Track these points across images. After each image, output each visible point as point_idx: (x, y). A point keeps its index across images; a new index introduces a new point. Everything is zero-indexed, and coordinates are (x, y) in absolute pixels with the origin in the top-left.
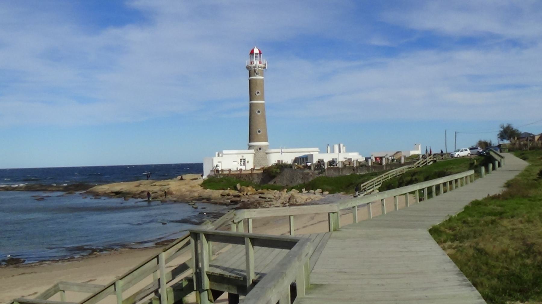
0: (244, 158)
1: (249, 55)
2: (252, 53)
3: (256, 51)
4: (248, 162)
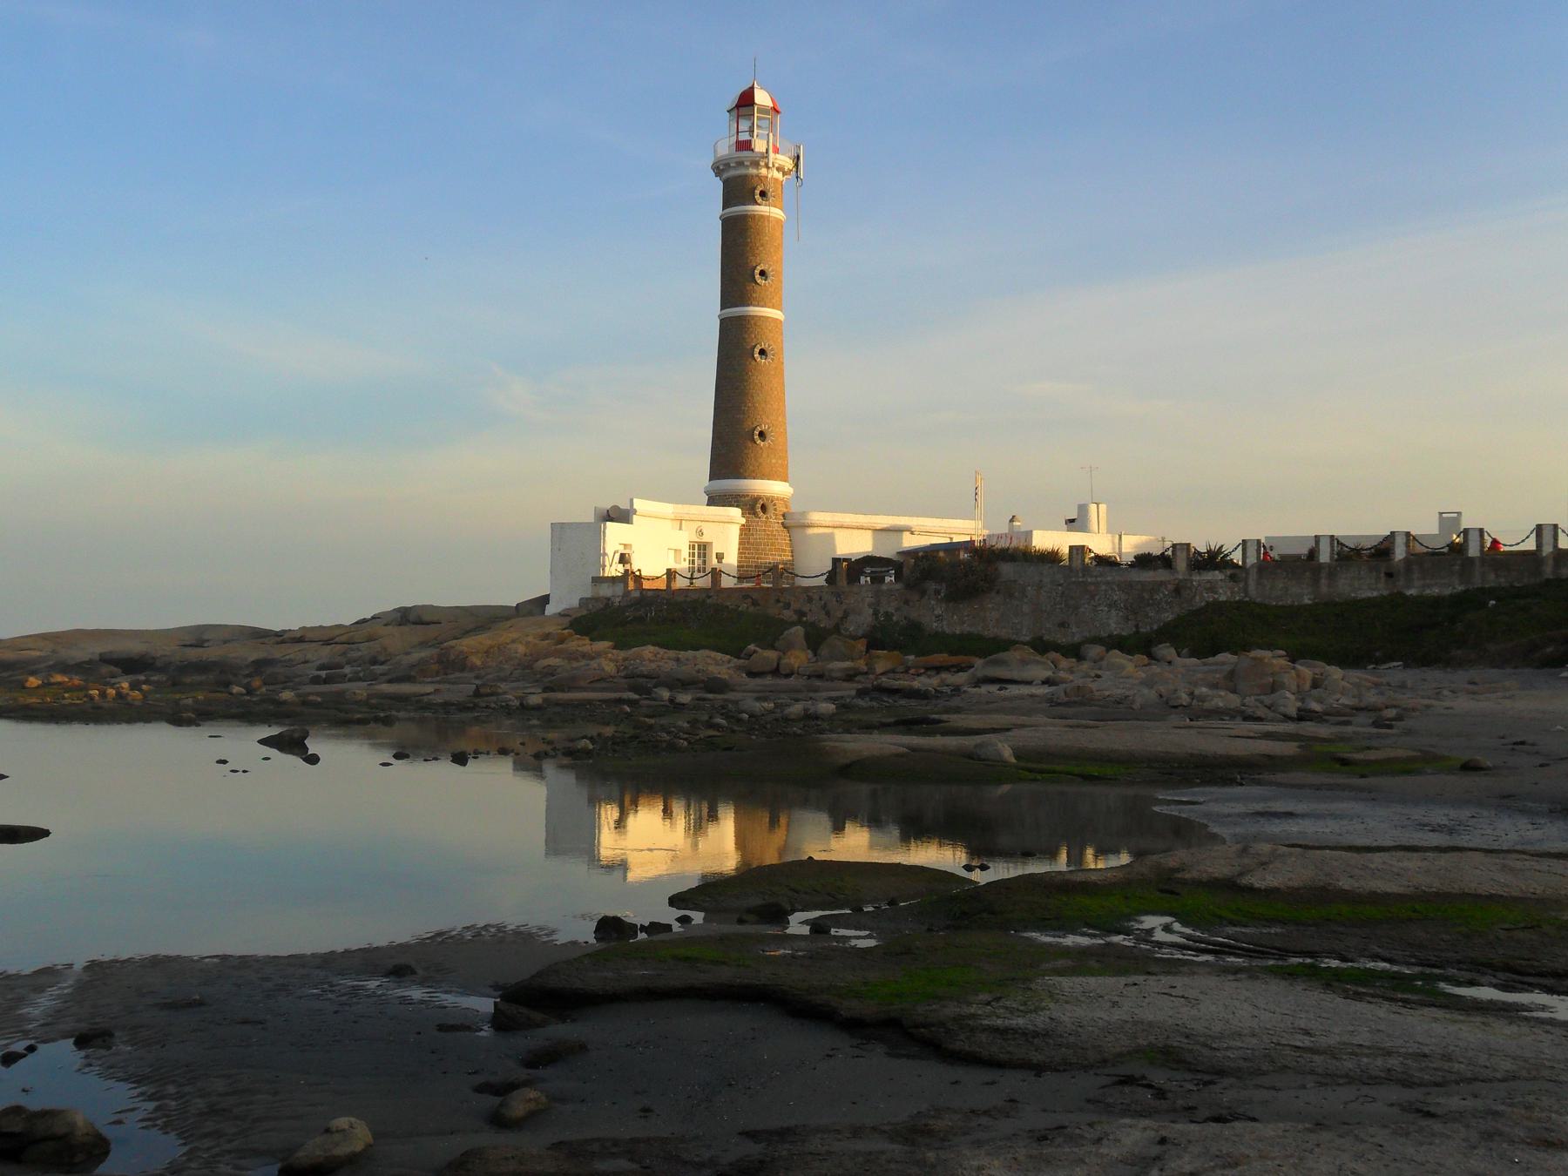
0: (705, 539)
3: (762, 98)
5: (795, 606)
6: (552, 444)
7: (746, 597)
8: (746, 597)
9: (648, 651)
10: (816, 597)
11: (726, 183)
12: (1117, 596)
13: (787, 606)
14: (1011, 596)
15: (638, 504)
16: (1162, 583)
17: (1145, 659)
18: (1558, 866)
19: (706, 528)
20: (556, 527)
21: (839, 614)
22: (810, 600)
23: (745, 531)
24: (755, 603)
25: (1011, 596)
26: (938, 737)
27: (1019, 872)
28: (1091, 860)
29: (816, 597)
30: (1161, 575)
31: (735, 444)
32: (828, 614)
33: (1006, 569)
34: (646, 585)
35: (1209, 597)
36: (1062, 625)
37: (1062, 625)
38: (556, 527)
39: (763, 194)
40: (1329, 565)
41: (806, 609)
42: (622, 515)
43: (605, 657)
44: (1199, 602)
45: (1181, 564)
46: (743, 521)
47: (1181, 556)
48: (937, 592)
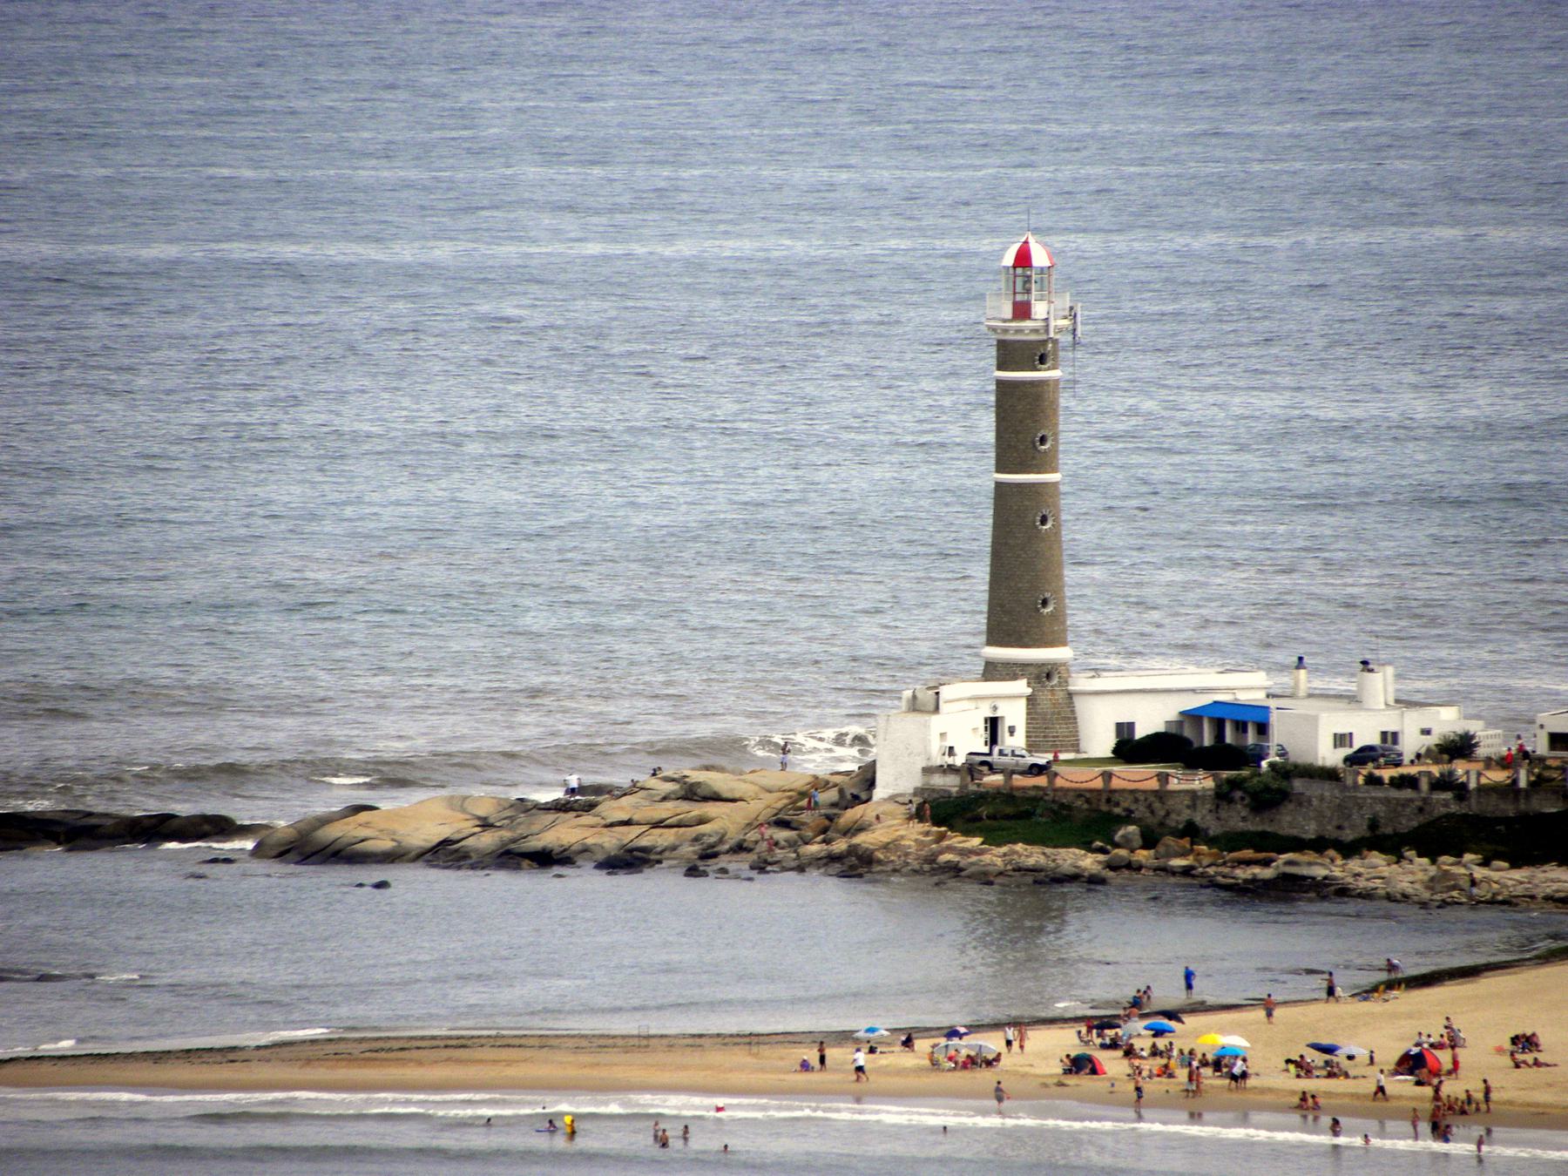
5: (1126, 805)
6: (492, 1170)
7: (1080, 796)
8: (1080, 796)
9: (1019, 847)
10: (1142, 798)
13: (1117, 804)
14: (1300, 804)
16: (1411, 800)
17: (1394, 858)
21: (1162, 813)
22: (1136, 800)
23: (1031, 700)
24: (1088, 801)
26: (672, 1030)
28: (1375, 1142)
29: (1142, 798)
30: (1408, 793)
31: (1021, 600)
32: (1152, 812)
33: (1298, 785)
35: (1443, 810)
36: (1339, 828)
37: (1339, 828)
40: (1525, 790)
41: (1133, 807)
43: (1139, 776)
44: (1436, 814)
45: (1424, 784)
46: (1030, 691)
48: (1242, 799)
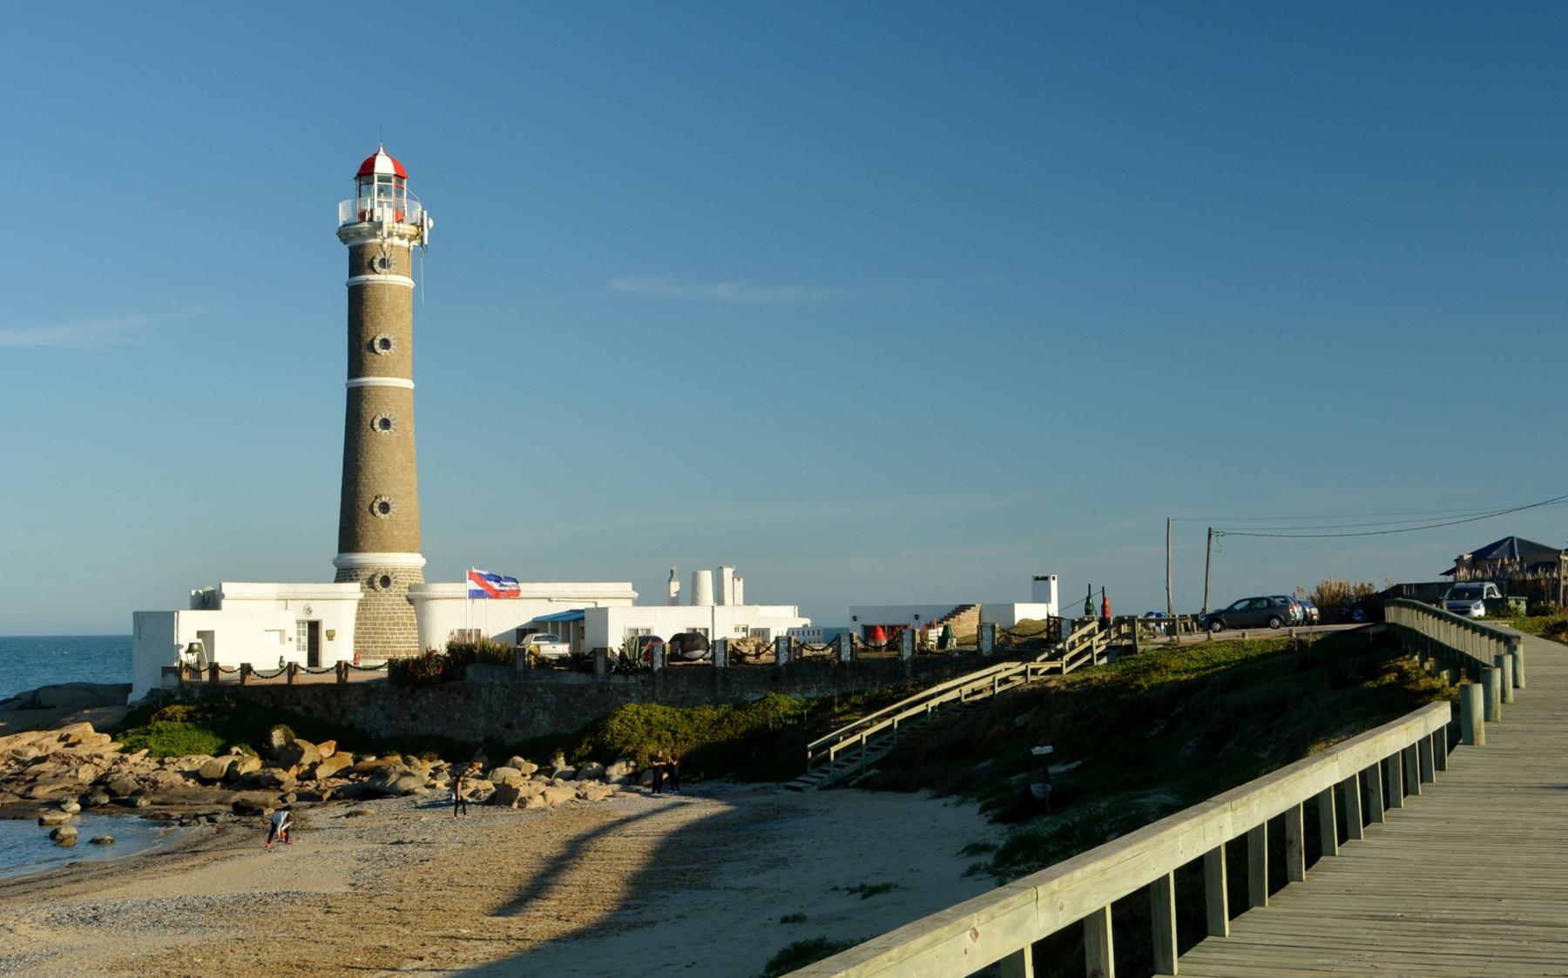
0: (313, 618)
1: (354, 184)
2: (367, 169)
3: (384, 165)
4: (331, 636)
5: (305, 703)
11: (351, 249)
12: (549, 698)
13: (298, 703)
14: (470, 697)
15: (227, 588)
18: (1558, 799)
19: (314, 605)
20: (137, 615)
23: (363, 605)
25: (470, 697)
27: (1029, 827)
34: (222, 676)
38: (137, 615)
39: (383, 263)
42: (209, 601)
46: (362, 595)
47: (600, 660)
